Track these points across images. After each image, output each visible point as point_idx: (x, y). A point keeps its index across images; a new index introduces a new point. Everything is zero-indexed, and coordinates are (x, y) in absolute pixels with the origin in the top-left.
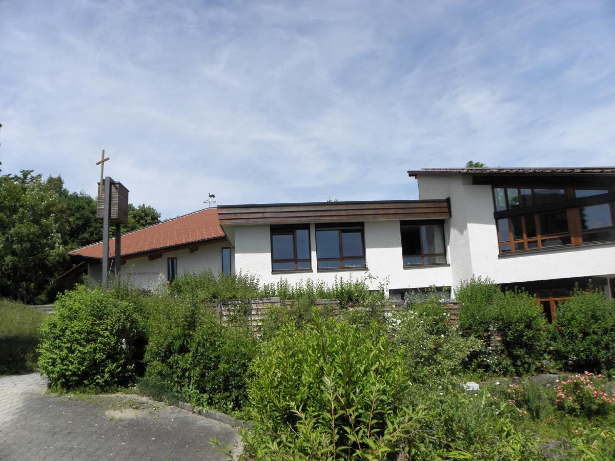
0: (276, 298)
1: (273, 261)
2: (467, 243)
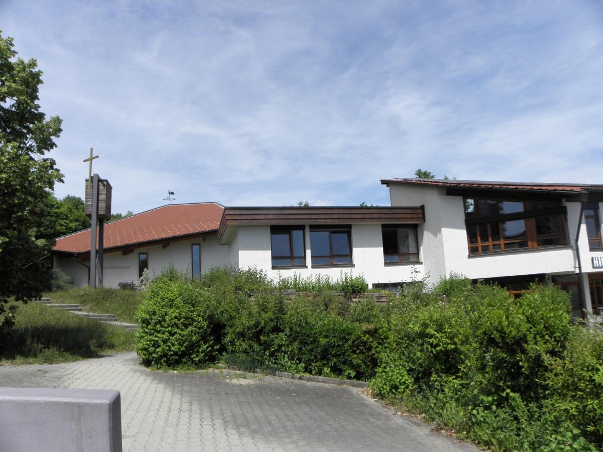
0: (292, 290)
1: (273, 258)
2: (441, 244)
